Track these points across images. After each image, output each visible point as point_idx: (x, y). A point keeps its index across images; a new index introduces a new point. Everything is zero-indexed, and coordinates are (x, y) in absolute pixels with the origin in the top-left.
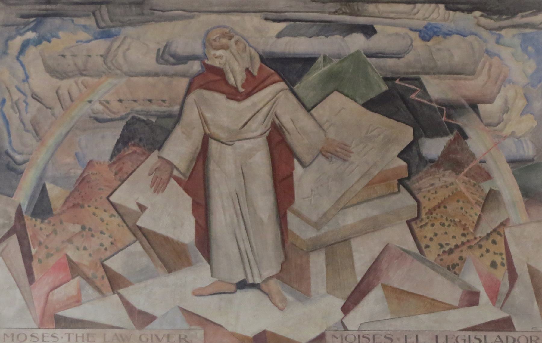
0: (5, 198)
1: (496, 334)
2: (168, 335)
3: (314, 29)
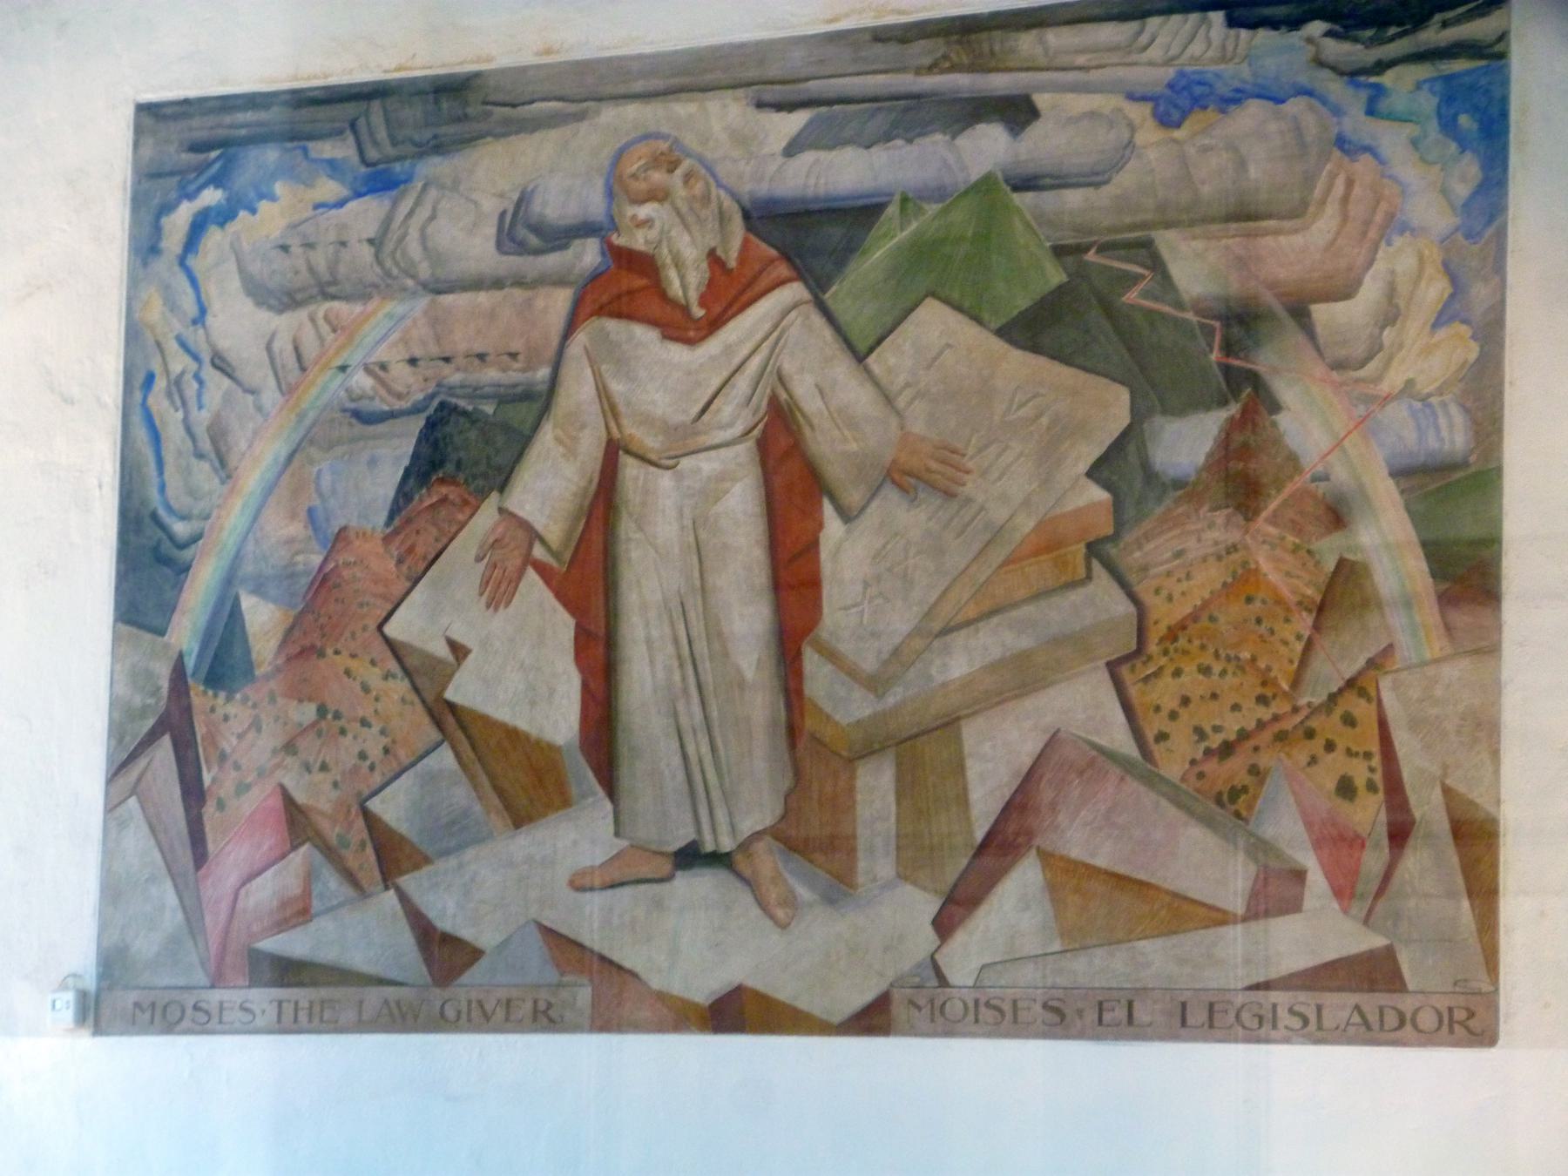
0: (148, 636)
1: (1352, 999)
2: (509, 1002)
3: (880, 122)
